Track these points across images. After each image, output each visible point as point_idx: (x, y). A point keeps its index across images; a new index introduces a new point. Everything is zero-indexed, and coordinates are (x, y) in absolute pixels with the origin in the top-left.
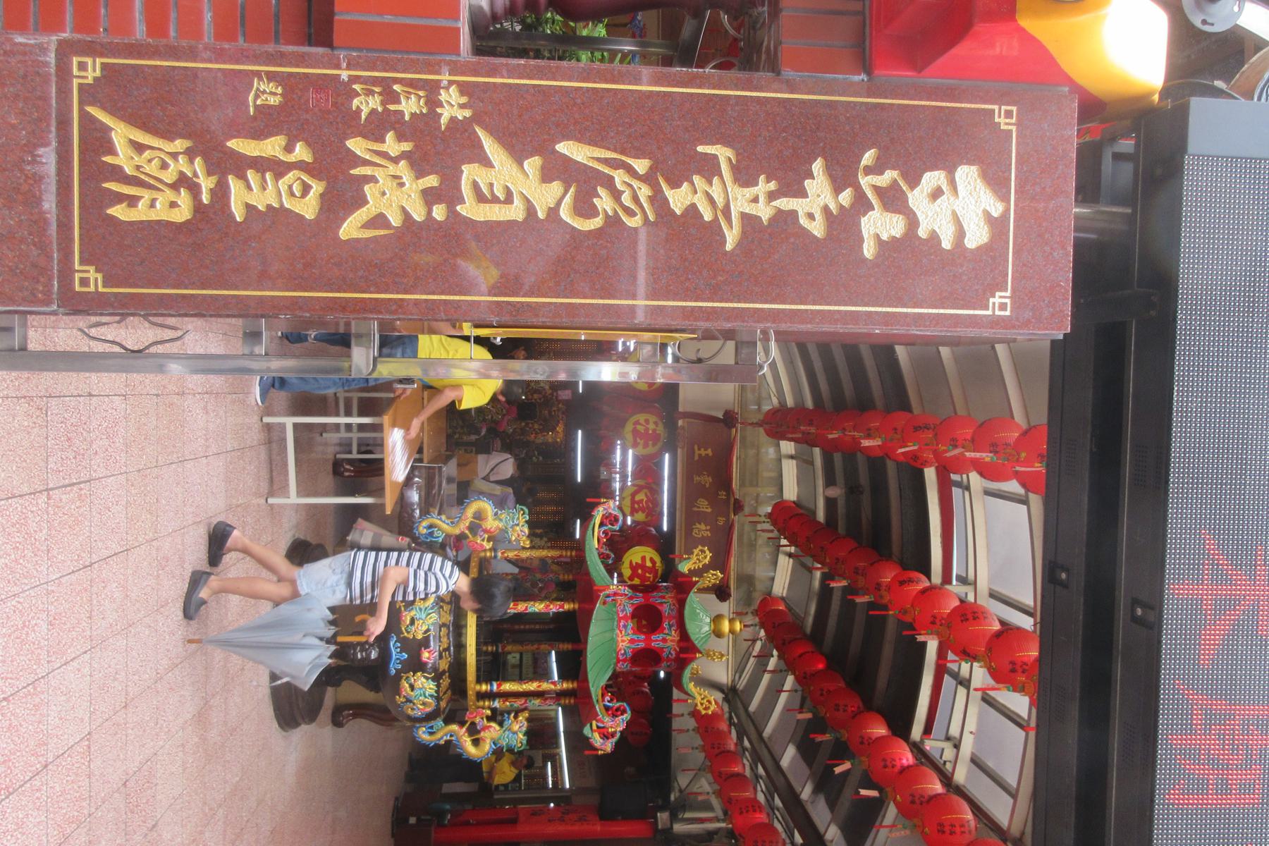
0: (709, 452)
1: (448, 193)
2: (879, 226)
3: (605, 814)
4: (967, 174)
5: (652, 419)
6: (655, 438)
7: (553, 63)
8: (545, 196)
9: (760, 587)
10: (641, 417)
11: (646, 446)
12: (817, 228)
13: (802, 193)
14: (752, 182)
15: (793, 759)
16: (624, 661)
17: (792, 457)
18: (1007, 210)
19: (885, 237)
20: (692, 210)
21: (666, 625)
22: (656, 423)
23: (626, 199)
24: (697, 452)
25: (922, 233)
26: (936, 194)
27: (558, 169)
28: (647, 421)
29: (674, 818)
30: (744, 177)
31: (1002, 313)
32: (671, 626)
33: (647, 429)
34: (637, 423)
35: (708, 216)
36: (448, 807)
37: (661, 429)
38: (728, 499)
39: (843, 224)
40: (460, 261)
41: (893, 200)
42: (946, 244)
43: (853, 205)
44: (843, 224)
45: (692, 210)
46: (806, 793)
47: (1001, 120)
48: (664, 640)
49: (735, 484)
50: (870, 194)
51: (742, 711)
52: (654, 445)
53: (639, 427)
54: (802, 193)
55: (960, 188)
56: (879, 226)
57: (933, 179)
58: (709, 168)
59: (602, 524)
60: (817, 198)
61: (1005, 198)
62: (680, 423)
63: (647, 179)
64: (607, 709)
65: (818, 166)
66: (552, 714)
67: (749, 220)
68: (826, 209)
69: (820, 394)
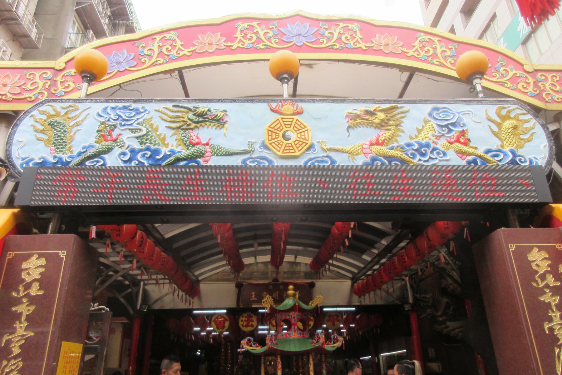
0: (253, 293)
2: (35, 291)
3: (409, 334)
5: (241, 319)
6: (249, 317)
9: (309, 269)
10: (241, 323)
11: (252, 321)
12: (32, 308)
13: (21, 314)
14: (15, 328)
15: (367, 255)
16: (303, 334)
17: (256, 258)
18: (37, 253)
19: (38, 288)
20: (20, 347)
21: (288, 317)
22: (243, 317)
23: (13, 368)
24: (253, 299)
25: (38, 277)
26: (29, 274)
28: (242, 321)
29: (407, 302)
30: (550, 320)
32: (289, 315)
33: (245, 321)
34: (243, 325)
35: (23, 342)
37: (245, 315)
38: (272, 284)
39: (32, 300)
41: (28, 286)
42: (43, 270)
43: (28, 298)
44: (32, 300)
45: (20, 347)
46: (376, 251)
47: (11, 257)
48: (294, 318)
49: (266, 282)
50: (26, 293)
51: (359, 275)
52: (252, 317)
53: (245, 324)
54: (21, 314)
55: (28, 267)
56: (35, 291)
57: (24, 276)
58: (9, 342)
59: (251, 346)
60: (24, 309)
61: (33, 254)
62: (241, 307)
63: (9, 361)
64: (318, 342)
65: (14, 309)
66: (384, 358)
67: (27, 328)
68: (27, 306)
69: (198, 262)
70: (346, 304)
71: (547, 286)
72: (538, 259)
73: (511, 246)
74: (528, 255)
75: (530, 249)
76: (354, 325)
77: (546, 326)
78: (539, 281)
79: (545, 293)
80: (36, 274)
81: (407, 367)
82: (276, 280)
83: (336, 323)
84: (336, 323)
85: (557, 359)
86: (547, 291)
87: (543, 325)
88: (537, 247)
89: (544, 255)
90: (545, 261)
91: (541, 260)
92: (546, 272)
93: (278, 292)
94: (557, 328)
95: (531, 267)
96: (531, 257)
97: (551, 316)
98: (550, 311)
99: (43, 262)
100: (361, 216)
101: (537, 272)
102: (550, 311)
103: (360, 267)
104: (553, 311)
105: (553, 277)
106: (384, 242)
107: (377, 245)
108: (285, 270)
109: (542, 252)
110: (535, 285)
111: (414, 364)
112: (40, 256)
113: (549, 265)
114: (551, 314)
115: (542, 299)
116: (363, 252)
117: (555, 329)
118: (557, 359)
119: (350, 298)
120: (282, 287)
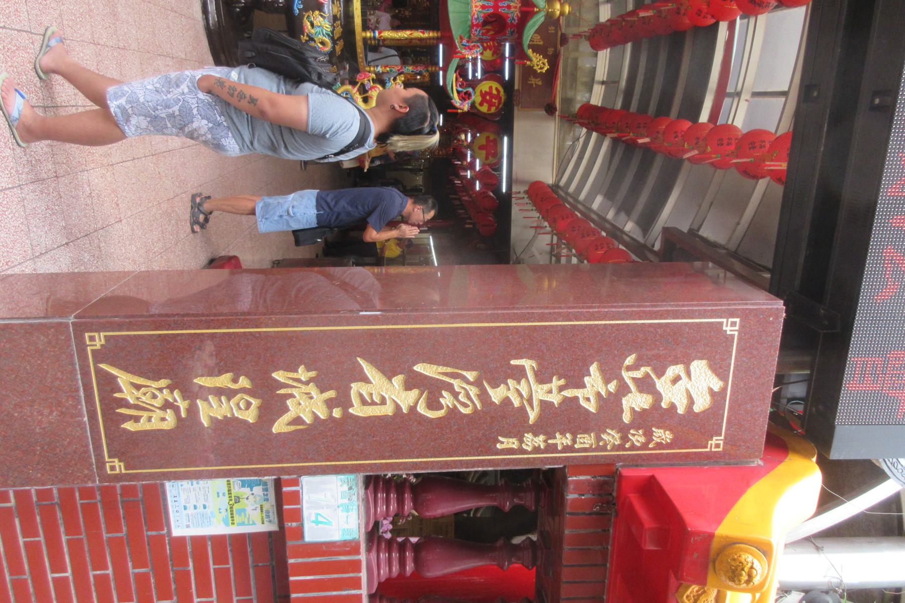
30: (542, 378)
38: (557, 32)
46: (610, 215)
66: (426, 241)
70: (514, 176)
71: (623, 389)
72: (692, 386)
73: (733, 324)
74: (704, 362)
75: (719, 370)
76: (478, 188)
77: (528, 364)
78: (638, 374)
79: (607, 381)
81: (424, 119)
82: (564, 40)
83: (484, 152)
84: (484, 152)
85: (449, 370)
86: (612, 387)
87: (530, 358)
88: (724, 390)
89: (702, 403)
90: (685, 401)
91: (688, 391)
92: (658, 397)
93: (541, 43)
94: (523, 387)
95: (676, 363)
96: (699, 367)
97: (550, 381)
98: (562, 382)
101: (660, 373)
102: (562, 382)
103: (579, 194)
104: (561, 389)
105: (644, 410)
106: (629, 226)
107: (623, 216)
108: (580, 63)
109: (708, 399)
110: (630, 360)
111: (432, 132)
113: (673, 407)
114: (556, 383)
115: (594, 368)
116: (610, 195)
117: (519, 383)
118: (449, 370)
119: (522, 182)
120: (551, 51)
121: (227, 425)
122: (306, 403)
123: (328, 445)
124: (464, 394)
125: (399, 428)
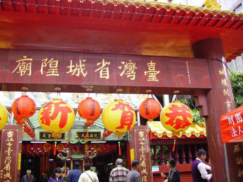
1: (8, 171)
2: (11, 140)
4: (8, 133)
7: (208, 141)
8: (9, 164)
27: (7, 163)
30: (141, 148)
31: (57, 64)
36: (141, 134)
39: (11, 142)
40: (205, 135)
41: (10, 139)
44: (11, 142)
56: (11, 140)
57: (8, 136)
58: (7, 152)
60: (10, 144)
75: (139, 131)
80: (11, 136)
99: (12, 132)
100: (126, 148)
112: (12, 131)
121: (147, 178)
122: (144, 171)
123: (149, 170)
124: (143, 156)
125: (147, 163)
